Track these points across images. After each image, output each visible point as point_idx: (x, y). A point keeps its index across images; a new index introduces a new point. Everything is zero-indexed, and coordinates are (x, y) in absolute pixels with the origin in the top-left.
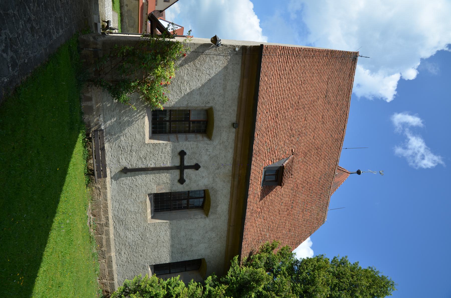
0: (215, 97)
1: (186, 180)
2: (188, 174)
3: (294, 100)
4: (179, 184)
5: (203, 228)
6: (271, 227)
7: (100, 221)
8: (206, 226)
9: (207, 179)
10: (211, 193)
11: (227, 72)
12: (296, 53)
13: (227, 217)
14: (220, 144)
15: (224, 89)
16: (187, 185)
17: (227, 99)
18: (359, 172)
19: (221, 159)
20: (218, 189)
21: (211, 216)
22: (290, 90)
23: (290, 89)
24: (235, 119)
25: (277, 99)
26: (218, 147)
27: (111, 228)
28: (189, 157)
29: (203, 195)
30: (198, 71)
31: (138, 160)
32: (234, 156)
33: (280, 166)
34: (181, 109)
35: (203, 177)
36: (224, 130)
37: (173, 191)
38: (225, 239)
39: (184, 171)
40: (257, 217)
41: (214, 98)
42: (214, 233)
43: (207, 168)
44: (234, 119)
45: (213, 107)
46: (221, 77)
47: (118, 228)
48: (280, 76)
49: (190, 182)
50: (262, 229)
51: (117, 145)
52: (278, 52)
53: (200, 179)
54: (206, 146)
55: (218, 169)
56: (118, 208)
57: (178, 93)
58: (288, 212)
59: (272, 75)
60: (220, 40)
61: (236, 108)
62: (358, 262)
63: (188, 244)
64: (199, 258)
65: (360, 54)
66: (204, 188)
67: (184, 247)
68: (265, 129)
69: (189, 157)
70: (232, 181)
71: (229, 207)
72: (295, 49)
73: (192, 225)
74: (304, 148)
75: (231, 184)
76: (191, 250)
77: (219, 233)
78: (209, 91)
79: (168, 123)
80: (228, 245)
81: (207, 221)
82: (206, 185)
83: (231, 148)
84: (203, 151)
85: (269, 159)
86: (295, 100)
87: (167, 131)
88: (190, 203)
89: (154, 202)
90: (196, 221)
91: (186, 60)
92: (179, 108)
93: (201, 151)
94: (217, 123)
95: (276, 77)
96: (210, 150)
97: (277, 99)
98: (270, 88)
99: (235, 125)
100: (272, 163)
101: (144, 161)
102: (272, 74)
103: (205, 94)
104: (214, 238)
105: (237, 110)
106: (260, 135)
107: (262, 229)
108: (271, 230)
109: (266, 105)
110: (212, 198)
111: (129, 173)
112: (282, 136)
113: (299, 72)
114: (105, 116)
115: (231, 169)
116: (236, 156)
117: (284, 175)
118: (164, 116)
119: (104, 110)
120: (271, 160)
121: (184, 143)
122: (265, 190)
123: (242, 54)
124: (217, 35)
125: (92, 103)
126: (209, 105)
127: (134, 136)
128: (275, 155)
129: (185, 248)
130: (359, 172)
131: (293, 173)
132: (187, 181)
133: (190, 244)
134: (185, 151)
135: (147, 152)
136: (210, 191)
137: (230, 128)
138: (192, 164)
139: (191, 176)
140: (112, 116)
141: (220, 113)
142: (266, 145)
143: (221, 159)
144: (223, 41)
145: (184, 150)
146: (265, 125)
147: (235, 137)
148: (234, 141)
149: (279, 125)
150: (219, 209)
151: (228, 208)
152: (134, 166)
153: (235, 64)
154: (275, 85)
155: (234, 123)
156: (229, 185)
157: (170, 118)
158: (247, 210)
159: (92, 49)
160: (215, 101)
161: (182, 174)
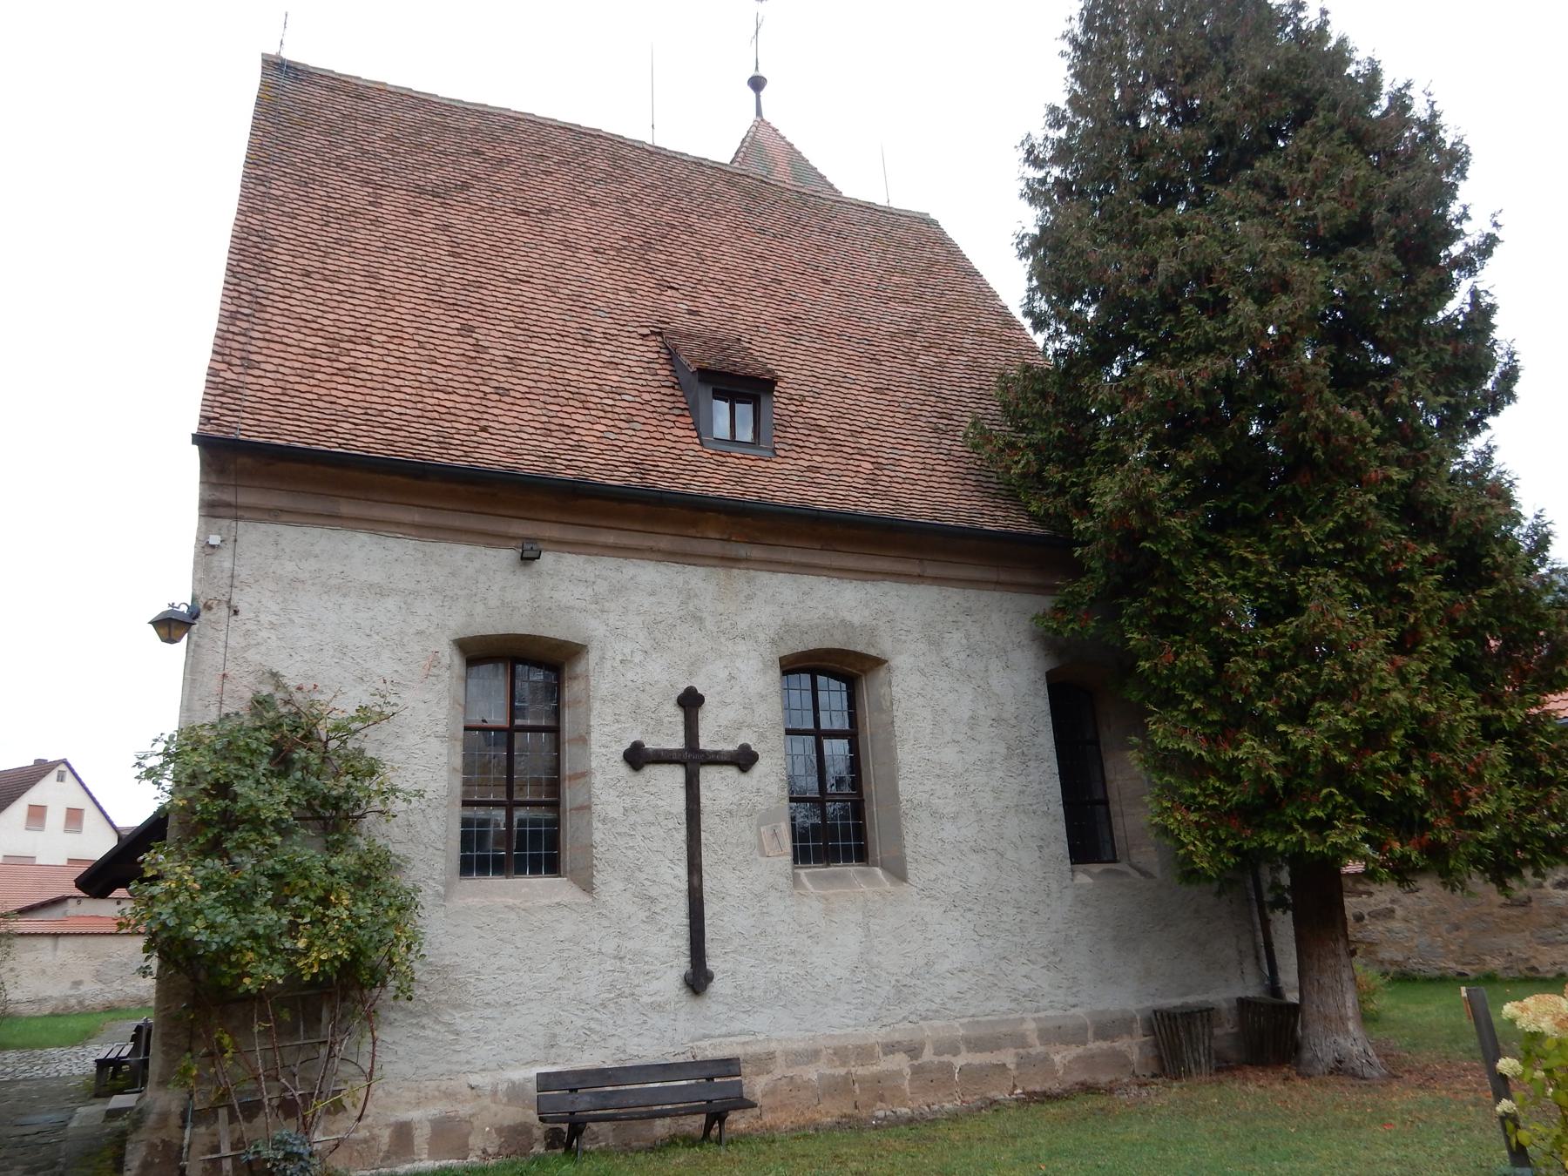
0: (412, 631)
1: (740, 743)
2: (717, 733)
3: (444, 323)
4: (759, 769)
6: (935, 420)
7: (899, 1073)
9: (739, 663)
13: (887, 586)
14: (602, 611)
15: (381, 592)
16: (762, 737)
18: (757, 84)
19: (662, 610)
20: (779, 622)
22: (400, 334)
23: (395, 334)
26: (613, 619)
28: (650, 730)
35: (732, 677)
38: (971, 593)
39: (704, 752)
40: (893, 474)
43: (695, 664)
46: (330, 605)
49: (749, 726)
50: (941, 456)
51: (597, 1015)
52: (234, 377)
53: (737, 689)
54: (608, 665)
55: (701, 620)
64: (1044, 691)
66: (776, 673)
68: (550, 439)
69: (650, 730)
71: (851, 579)
72: (227, 307)
76: (1013, 722)
78: (386, 654)
79: (519, 814)
82: (761, 666)
83: (618, 569)
84: (630, 675)
88: (837, 726)
89: (828, 866)
92: (454, 769)
94: (518, 624)
96: (627, 651)
98: (385, 414)
100: (686, 413)
104: (967, 637)
105: (468, 543)
106: (569, 457)
107: (941, 456)
108: (946, 422)
114: (479, 1064)
116: (651, 550)
117: (732, 368)
118: (491, 829)
119: (450, 1072)
122: (790, 442)
127: (561, 946)
128: (654, 403)
129: (1004, 745)
130: (757, 84)
131: (735, 335)
132: (747, 738)
134: (627, 745)
135: (628, 895)
137: (540, 574)
140: (478, 1038)
142: (612, 436)
144: (179, 593)
145: (623, 749)
146: (534, 437)
148: (592, 558)
149: (539, 384)
150: (856, 619)
152: (683, 944)
153: (280, 547)
156: (764, 578)
157: (496, 804)
158: (864, 510)
161: (716, 759)
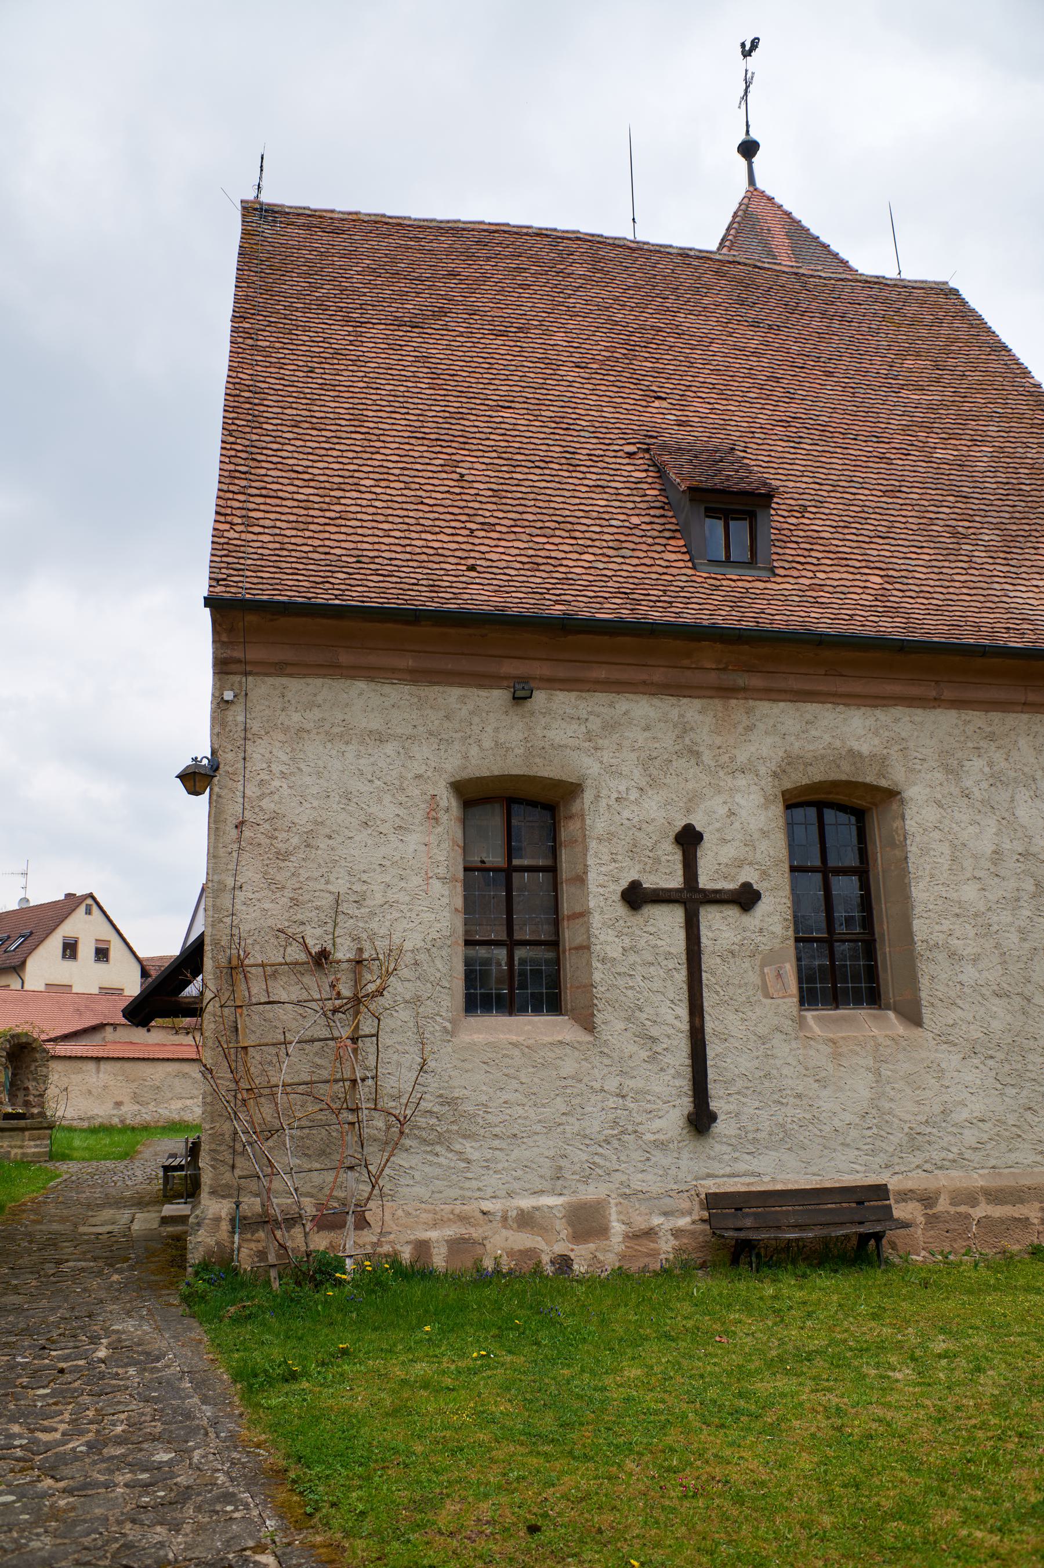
4: (763, 907)
5: (949, 810)
8: (939, 796)
9: (738, 798)
10: (798, 778)
11: (315, 731)
12: (243, 462)
13: (898, 711)
14: (596, 749)
16: (765, 875)
17: (421, 729)
19: (657, 745)
20: (781, 754)
21: (897, 775)
24: (496, 693)
25: (419, 528)
26: (607, 756)
27: (944, 1182)
28: (648, 869)
29: (812, 812)
30: (313, 843)
31: (662, 1070)
32: (645, 694)
33: (688, 503)
34: (459, 903)
35: (731, 813)
36: (541, 735)
37: (791, 933)
38: (996, 716)
39: (703, 891)
41: (418, 777)
42: (966, 763)
43: (693, 800)
44: (499, 696)
45: (453, 780)
46: (334, 753)
47: (943, 1154)
48: (331, 522)
49: (750, 864)
52: (237, 535)
54: (603, 803)
55: (698, 754)
56: (856, 1153)
57: (397, 915)
58: (893, 456)
59: (326, 553)
60: (195, 759)
61: (456, 692)
62: (184, 777)
63: (1019, 871)
65: (250, 196)
66: (777, 810)
67: (1029, 886)
69: (648, 869)
70: (746, 698)
71: (859, 706)
73: (932, 853)
74: (624, 406)
75: (761, 700)
77: (970, 745)
78: (387, 798)
80: (1024, 704)
81: (915, 793)
82: (762, 800)
83: (611, 705)
84: (626, 814)
85: (663, 548)
86: (425, 454)
87: (550, 955)
89: (837, 1008)
90: (918, 839)
91: (273, 887)
92: (456, 910)
93: (625, 822)
94: (513, 765)
95: (332, 537)
96: (623, 788)
97: (419, 528)
99: (519, 694)
100: (678, 535)
101: (665, 1046)
102: (323, 557)
103: (401, 814)
104: (991, 764)
109: (442, 572)
110: (817, 774)
111: (711, 1104)
112: (568, 501)
113: (317, 445)
115: (697, 703)
116: (644, 683)
119: (463, 1197)
120: (663, 541)
121: (592, 887)
123: (246, 674)
124: (176, 774)
125: (437, 1241)
126: (445, 797)
128: (644, 527)
129: (1032, 881)
131: (727, 444)
132: (748, 875)
133: (1018, 860)
134: (624, 884)
136: (788, 785)
138: (678, 857)
139: (725, 861)
141: (474, 751)
142: (601, 565)
143: (657, 745)
147: (568, 691)
148: (584, 694)
151: (863, 709)
152: (685, 1083)
153: (286, 699)
154: (365, 539)
155: (514, 698)
156: (764, 707)
159: (236, 1237)
160: (429, 773)
161: (717, 898)
